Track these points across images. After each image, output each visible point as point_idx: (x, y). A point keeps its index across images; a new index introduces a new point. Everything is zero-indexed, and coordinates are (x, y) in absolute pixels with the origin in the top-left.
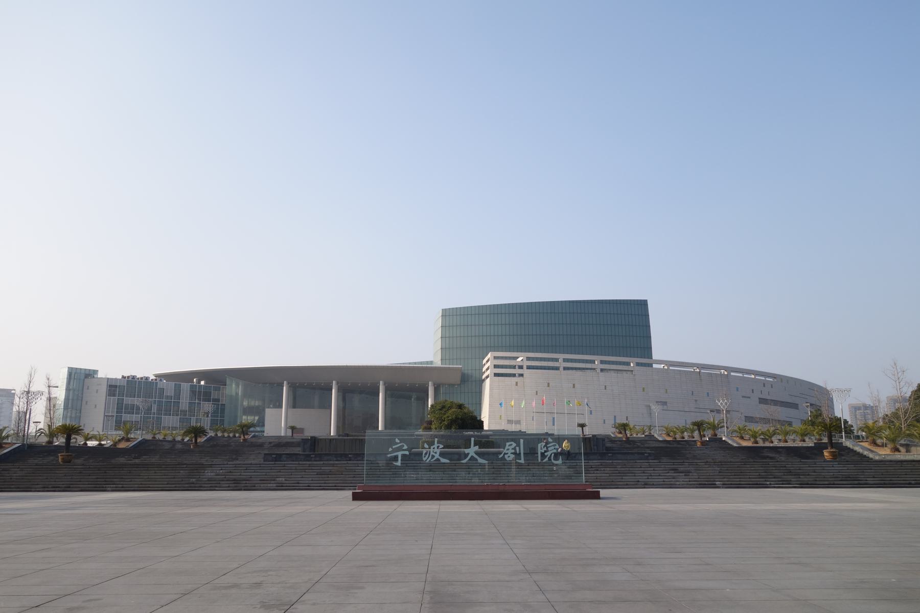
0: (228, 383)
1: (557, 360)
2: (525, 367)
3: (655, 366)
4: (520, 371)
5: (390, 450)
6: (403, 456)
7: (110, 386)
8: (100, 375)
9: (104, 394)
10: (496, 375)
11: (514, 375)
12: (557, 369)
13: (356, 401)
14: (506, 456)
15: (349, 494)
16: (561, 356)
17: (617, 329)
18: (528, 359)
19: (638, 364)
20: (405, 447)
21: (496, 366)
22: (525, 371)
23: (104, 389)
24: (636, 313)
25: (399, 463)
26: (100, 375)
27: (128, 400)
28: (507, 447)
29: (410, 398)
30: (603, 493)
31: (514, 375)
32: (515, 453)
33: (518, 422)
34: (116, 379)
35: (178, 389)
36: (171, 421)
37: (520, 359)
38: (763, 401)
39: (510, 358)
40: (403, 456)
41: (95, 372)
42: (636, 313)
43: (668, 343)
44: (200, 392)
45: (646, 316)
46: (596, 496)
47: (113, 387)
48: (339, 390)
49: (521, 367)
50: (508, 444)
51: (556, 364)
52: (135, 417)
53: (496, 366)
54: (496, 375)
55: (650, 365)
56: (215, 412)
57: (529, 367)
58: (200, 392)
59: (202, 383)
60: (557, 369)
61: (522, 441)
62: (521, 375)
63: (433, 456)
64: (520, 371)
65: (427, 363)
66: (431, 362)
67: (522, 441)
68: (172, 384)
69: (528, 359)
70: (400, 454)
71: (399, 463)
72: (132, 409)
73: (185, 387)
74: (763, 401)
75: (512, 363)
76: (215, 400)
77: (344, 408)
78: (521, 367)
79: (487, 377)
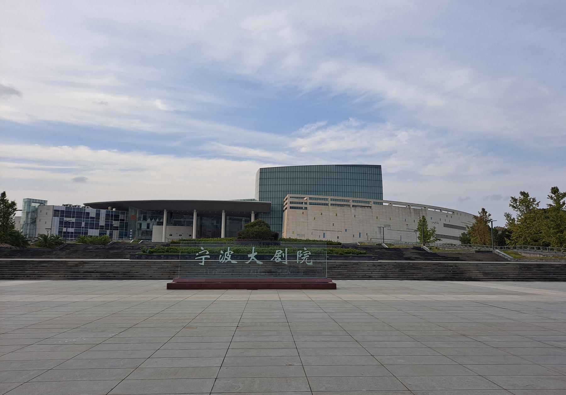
0: (130, 210)
1: (327, 199)
2: (308, 203)
3: (384, 204)
4: (306, 206)
5: (197, 254)
6: (206, 259)
7: (55, 210)
8: (49, 204)
9: (51, 215)
10: (291, 208)
11: (301, 208)
12: (327, 205)
13: (208, 222)
14: (276, 259)
15: (164, 283)
16: (329, 198)
17: (362, 181)
18: (310, 198)
19: (374, 203)
20: (208, 253)
21: (291, 203)
22: (308, 206)
23: (51, 213)
24: (374, 172)
25: (203, 264)
26: (49, 204)
27: (66, 219)
28: (276, 253)
29: (241, 220)
30: (339, 283)
31: (301, 208)
32: (281, 257)
33: (304, 235)
34: (59, 206)
35: (98, 215)
36: (94, 232)
37: (305, 199)
38: (446, 225)
39: (345, 201)
40: (206, 259)
41: (46, 202)
42: (374, 172)
43: (391, 190)
44: (112, 215)
45: (380, 174)
46: (334, 287)
47: (57, 212)
48: (198, 215)
49: (306, 203)
50: (277, 251)
51: (327, 202)
52: (71, 230)
53: (291, 203)
54: (291, 208)
55: (381, 204)
56: (121, 226)
57: (311, 204)
58: (112, 215)
59: (114, 210)
60: (327, 205)
61: (286, 249)
62: (306, 208)
63: (226, 259)
64: (306, 206)
65: (251, 200)
66: (254, 200)
67: (286, 249)
68: (94, 210)
69: (310, 198)
70: (203, 257)
71: (203, 264)
72: (68, 225)
73: (103, 212)
74: (446, 225)
75: (301, 201)
76: (121, 220)
77: (201, 226)
78: (306, 203)
79: (286, 209)
